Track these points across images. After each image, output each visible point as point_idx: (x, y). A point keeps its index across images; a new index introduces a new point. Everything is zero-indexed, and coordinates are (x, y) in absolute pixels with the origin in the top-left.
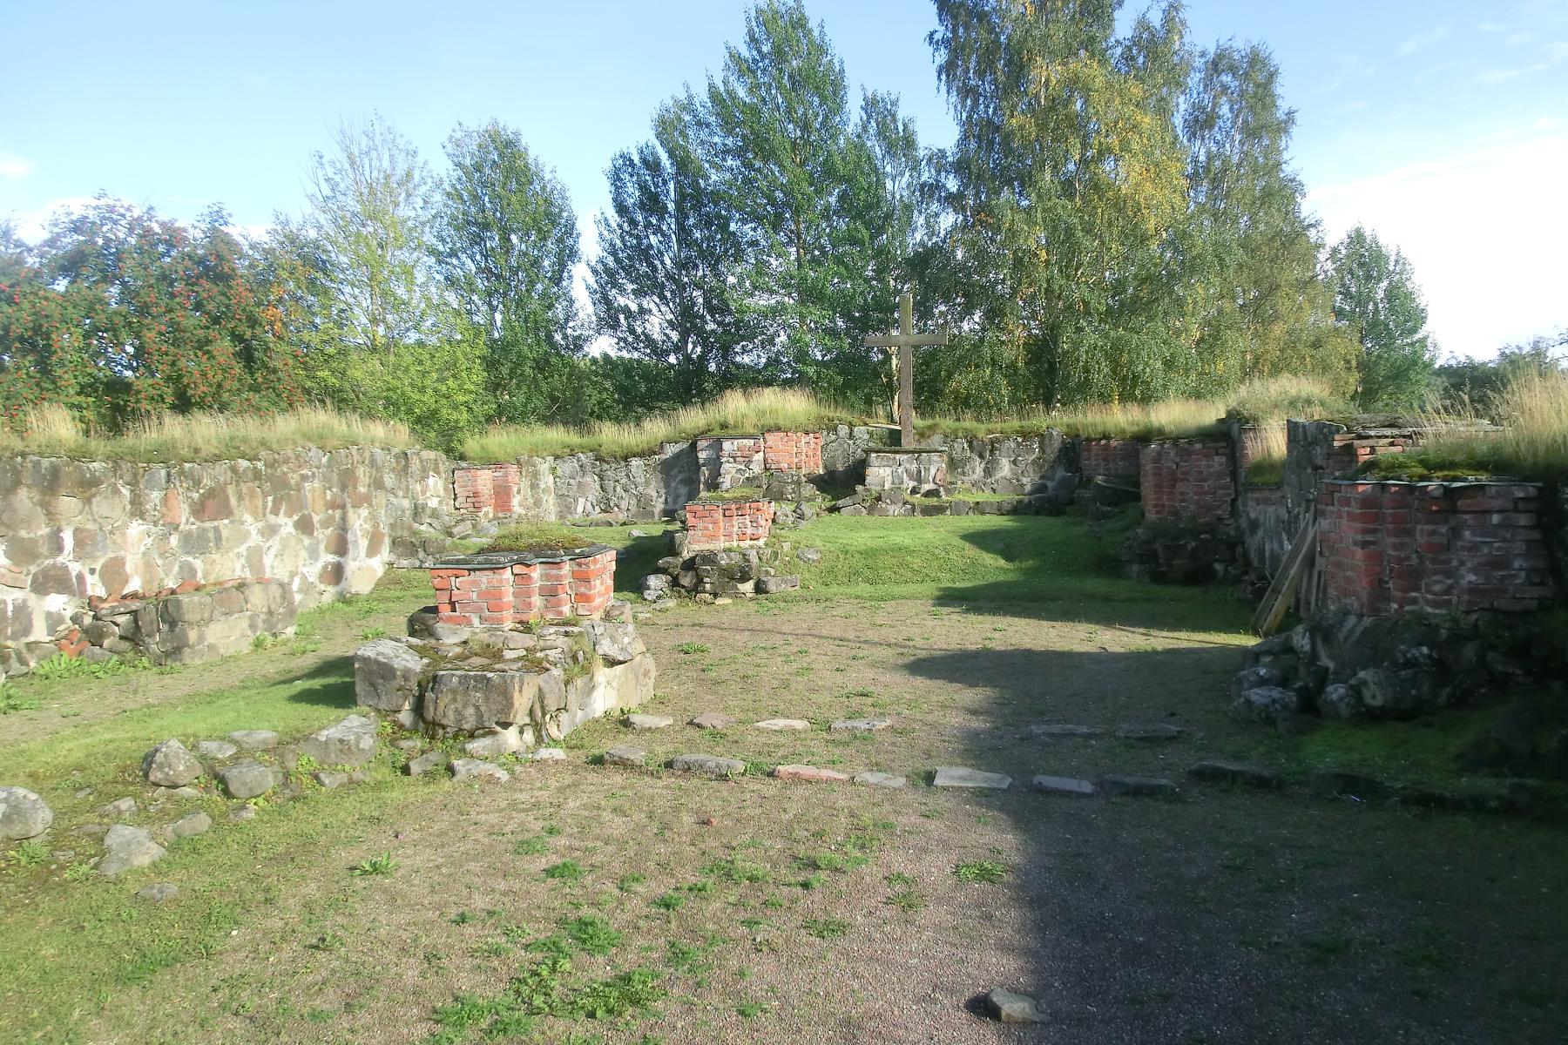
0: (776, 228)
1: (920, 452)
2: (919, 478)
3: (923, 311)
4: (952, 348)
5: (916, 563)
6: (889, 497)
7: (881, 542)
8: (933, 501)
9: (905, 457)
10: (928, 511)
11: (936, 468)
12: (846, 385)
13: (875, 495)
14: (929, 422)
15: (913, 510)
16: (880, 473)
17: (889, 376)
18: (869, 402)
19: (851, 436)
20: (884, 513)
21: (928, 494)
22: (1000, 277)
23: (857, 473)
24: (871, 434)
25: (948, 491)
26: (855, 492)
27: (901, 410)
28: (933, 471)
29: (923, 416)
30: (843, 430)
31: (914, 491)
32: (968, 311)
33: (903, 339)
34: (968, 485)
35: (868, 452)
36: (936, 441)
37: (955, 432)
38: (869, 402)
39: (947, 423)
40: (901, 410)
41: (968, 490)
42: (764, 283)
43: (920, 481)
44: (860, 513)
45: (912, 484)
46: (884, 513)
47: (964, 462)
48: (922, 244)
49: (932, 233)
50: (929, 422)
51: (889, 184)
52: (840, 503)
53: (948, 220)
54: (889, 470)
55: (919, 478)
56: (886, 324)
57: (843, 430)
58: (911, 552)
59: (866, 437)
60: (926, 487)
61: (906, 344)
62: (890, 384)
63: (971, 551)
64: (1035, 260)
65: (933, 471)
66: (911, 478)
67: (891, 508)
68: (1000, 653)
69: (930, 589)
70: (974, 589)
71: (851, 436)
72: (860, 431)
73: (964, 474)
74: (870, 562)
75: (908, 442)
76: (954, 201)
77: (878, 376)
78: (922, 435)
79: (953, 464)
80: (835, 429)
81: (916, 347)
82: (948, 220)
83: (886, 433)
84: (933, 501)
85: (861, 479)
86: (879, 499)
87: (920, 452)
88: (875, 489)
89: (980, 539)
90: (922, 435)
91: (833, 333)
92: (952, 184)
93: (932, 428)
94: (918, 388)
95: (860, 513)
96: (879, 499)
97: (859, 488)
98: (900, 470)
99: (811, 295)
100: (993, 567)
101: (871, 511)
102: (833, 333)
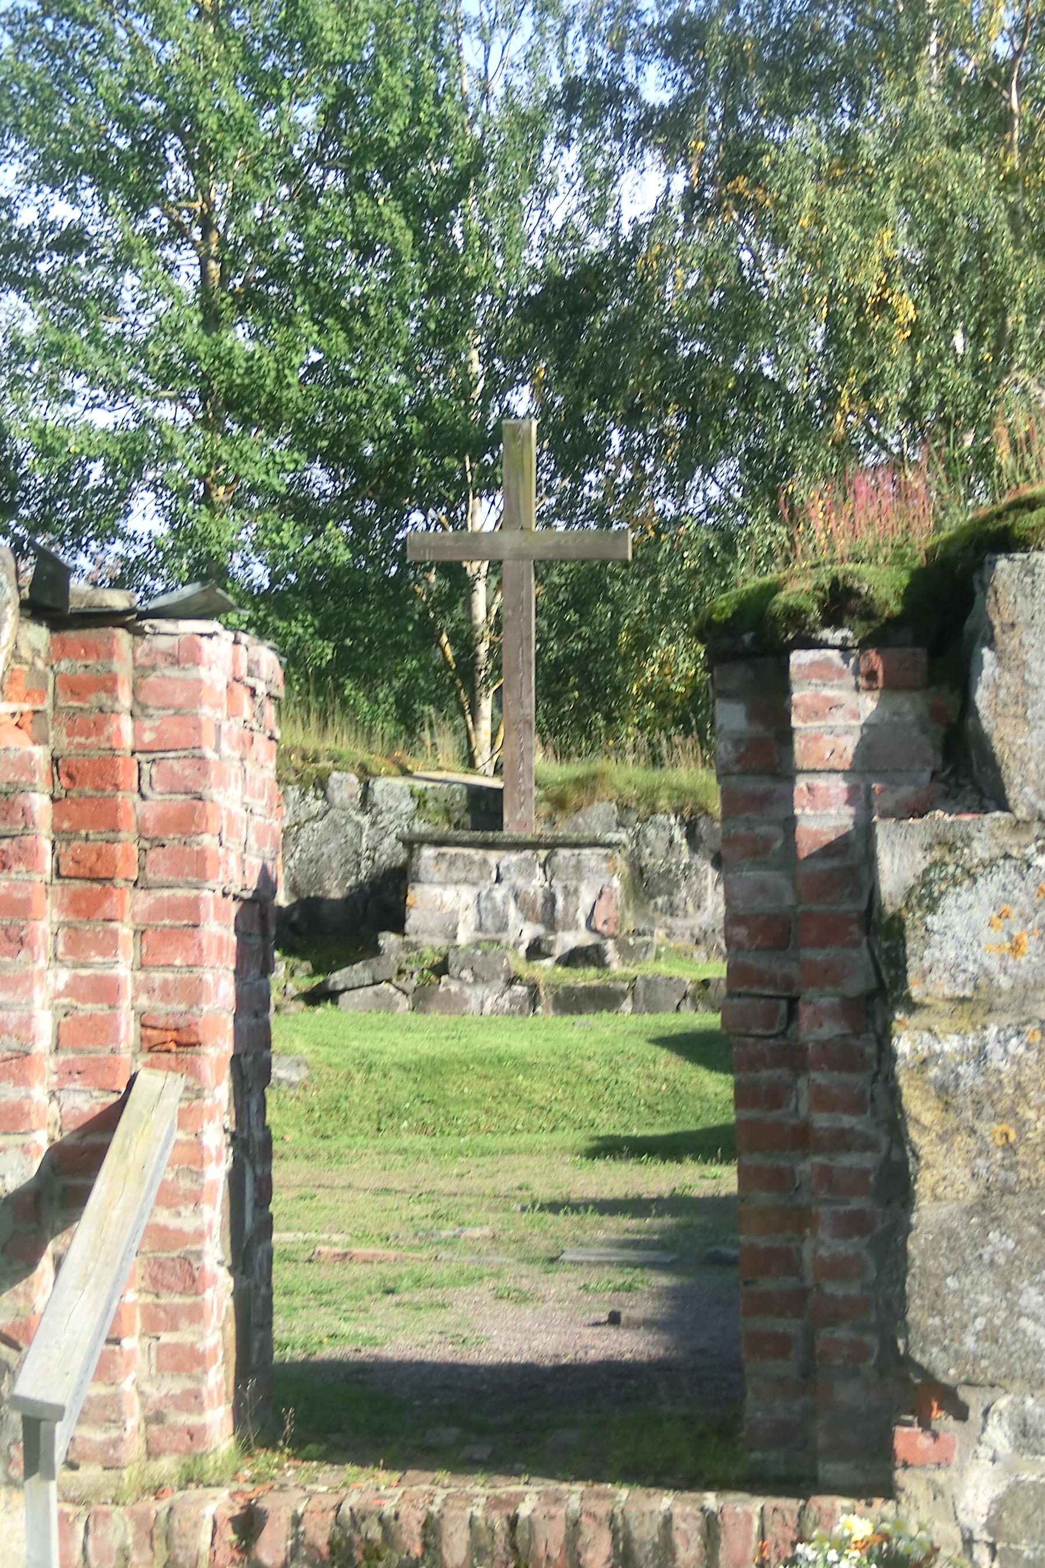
0: (137, 204)
1: (553, 846)
2: (548, 915)
3: (572, 448)
4: (645, 565)
5: (541, 1090)
6: (469, 963)
7: (454, 1047)
8: (586, 977)
9: (512, 858)
10: (571, 1002)
11: (595, 887)
12: (345, 663)
13: (431, 958)
14: (576, 769)
15: (534, 997)
16: (446, 902)
17: (465, 643)
18: (408, 721)
19: (365, 801)
20: (454, 1004)
21: (574, 958)
22: (793, 363)
23: (381, 902)
24: (421, 800)
25: (627, 952)
26: (376, 950)
27: (494, 741)
28: (587, 897)
29: (563, 754)
30: (345, 786)
31: (536, 951)
32: (691, 458)
33: (510, 541)
34: (684, 942)
35: (411, 843)
36: (597, 817)
37: (649, 797)
38: (408, 721)
39: (626, 772)
40: (494, 741)
41: (683, 954)
42: (662, 697)
43: (551, 922)
44: (390, 1006)
45: (530, 931)
46: (454, 1004)
47: (669, 882)
48: (568, 236)
49: (598, 213)
50: (576, 769)
51: (471, 50)
52: (338, 978)
53: (645, 188)
54: (467, 894)
55: (548, 915)
56: (451, 496)
57: (345, 786)
58: (523, 1066)
59: (408, 805)
60: (568, 940)
61: (520, 556)
62: (467, 666)
63: (671, 1066)
64: (878, 323)
65: (587, 897)
66: (527, 910)
67: (475, 994)
68: (704, 1199)
69: (580, 1139)
70: (675, 1136)
71: (365, 801)
72: (389, 788)
73: (671, 910)
74: (427, 1089)
75: (521, 818)
76: (667, 129)
77: (428, 636)
78: (559, 803)
79: (643, 884)
80: (321, 783)
81: (543, 567)
82: (645, 188)
83: (460, 799)
84: (586, 977)
85: (395, 919)
86: (441, 969)
87: (553, 846)
88: (432, 945)
89: (690, 1046)
90: (559, 803)
91: (300, 508)
92: (655, 85)
93: (587, 784)
94: (551, 680)
95: (390, 1006)
96: (441, 969)
97: (388, 940)
98: (500, 892)
99: (234, 402)
100: (713, 1093)
101: (421, 999)
102: (300, 508)
